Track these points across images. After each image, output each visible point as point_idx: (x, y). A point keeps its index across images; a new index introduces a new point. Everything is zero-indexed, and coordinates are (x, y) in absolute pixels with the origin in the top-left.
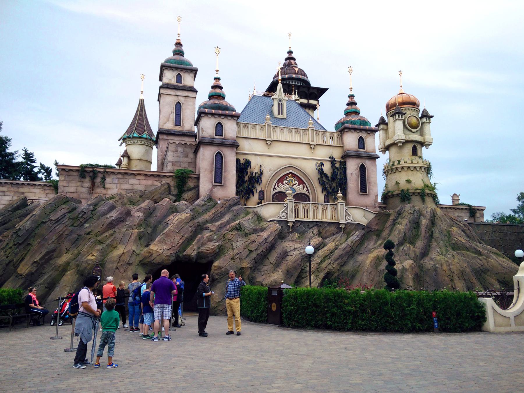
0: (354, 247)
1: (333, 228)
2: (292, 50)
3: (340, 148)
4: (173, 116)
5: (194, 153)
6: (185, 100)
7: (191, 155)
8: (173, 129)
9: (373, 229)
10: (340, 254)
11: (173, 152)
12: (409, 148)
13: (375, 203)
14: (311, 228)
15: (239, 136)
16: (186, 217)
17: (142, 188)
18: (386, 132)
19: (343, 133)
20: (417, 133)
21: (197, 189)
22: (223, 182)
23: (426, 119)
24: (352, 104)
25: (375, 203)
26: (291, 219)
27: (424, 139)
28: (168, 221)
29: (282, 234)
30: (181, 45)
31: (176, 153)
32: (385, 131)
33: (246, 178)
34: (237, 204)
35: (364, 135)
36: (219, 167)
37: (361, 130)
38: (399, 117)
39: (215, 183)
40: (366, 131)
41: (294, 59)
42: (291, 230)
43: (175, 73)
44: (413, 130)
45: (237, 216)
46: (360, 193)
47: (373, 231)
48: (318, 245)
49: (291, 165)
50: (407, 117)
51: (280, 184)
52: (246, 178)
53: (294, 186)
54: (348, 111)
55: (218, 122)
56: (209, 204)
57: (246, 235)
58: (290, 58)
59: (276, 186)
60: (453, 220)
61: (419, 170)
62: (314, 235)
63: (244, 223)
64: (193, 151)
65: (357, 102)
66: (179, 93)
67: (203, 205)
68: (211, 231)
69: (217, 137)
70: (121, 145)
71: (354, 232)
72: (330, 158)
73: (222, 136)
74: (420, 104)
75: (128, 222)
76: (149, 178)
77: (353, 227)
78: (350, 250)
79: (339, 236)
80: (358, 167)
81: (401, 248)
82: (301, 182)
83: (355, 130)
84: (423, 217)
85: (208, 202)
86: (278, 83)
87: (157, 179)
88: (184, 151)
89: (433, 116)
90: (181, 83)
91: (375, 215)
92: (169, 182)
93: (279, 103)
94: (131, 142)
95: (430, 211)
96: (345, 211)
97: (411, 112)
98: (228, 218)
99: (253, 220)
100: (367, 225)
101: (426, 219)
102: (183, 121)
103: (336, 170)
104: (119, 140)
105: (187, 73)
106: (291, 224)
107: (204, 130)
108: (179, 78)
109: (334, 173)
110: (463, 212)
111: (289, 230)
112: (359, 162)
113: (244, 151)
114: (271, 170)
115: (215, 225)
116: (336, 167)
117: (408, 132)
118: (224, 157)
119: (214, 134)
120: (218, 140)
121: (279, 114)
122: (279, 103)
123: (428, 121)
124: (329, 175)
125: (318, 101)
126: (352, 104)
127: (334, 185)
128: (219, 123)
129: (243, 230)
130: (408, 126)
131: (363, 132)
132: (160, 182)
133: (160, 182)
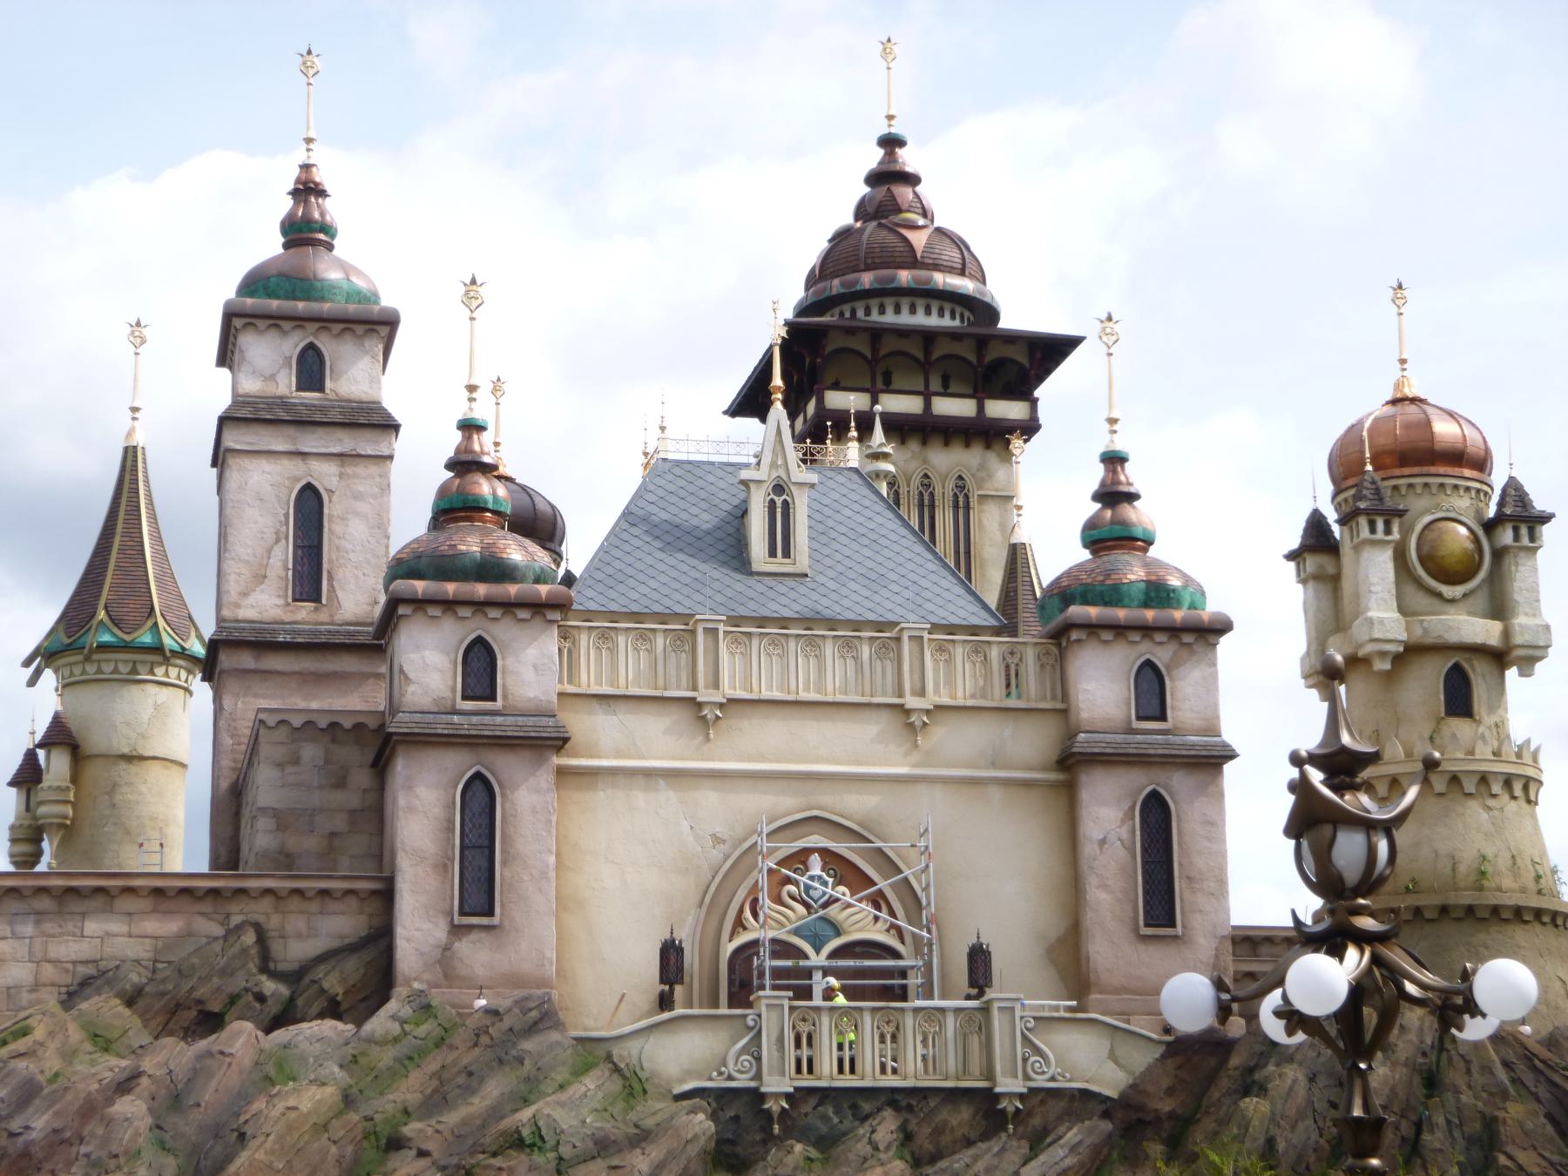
1: (961, 1118)
4: (283, 556)
5: (375, 764)
6: (341, 475)
7: (362, 778)
8: (288, 617)
12: (1426, 683)
15: (571, 689)
16: (319, 1101)
20: (1471, 600)
21: (382, 944)
22: (498, 910)
23: (1516, 530)
24: (1113, 496)
26: (778, 1084)
27: (1506, 634)
28: (246, 1122)
30: (322, 193)
34: (541, 1026)
35: (1161, 654)
37: (1147, 630)
38: (1373, 530)
39: (462, 913)
40: (1174, 631)
41: (912, 180)
43: (293, 344)
44: (1447, 591)
45: (537, 1079)
49: (815, 813)
54: (1104, 533)
55: (472, 636)
56: (422, 1030)
59: (748, 914)
61: (1473, 791)
63: (558, 1114)
64: (370, 755)
65: (1137, 486)
66: (312, 441)
67: (396, 1040)
68: (422, 1154)
69: (469, 705)
70: (32, 682)
71: (1062, 1129)
75: (88, 1143)
77: (1054, 1108)
79: (989, 1149)
80: (1132, 808)
83: (1120, 630)
85: (417, 1025)
86: (771, 403)
87: (207, 907)
88: (327, 761)
90: (321, 389)
92: (261, 919)
93: (772, 502)
94: (84, 672)
96: (1023, 1035)
98: (496, 1093)
99: (600, 1095)
100: (1123, 1095)
101: (1394, 1064)
102: (331, 578)
104: (27, 663)
105: (348, 337)
108: (311, 370)
112: (1139, 782)
113: (591, 756)
114: (724, 842)
115: (439, 1127)
117: (1419, 600)
120: (475, 719)
121: (773, 553)
122: (772, 502)
123: (1525, 541)
125: (1034, 402)
126: (1113, 496)
128: (480, 642)
129: (548, 1146)
131: (1160, 637)
132: (221, 917)
133: (221, 917)
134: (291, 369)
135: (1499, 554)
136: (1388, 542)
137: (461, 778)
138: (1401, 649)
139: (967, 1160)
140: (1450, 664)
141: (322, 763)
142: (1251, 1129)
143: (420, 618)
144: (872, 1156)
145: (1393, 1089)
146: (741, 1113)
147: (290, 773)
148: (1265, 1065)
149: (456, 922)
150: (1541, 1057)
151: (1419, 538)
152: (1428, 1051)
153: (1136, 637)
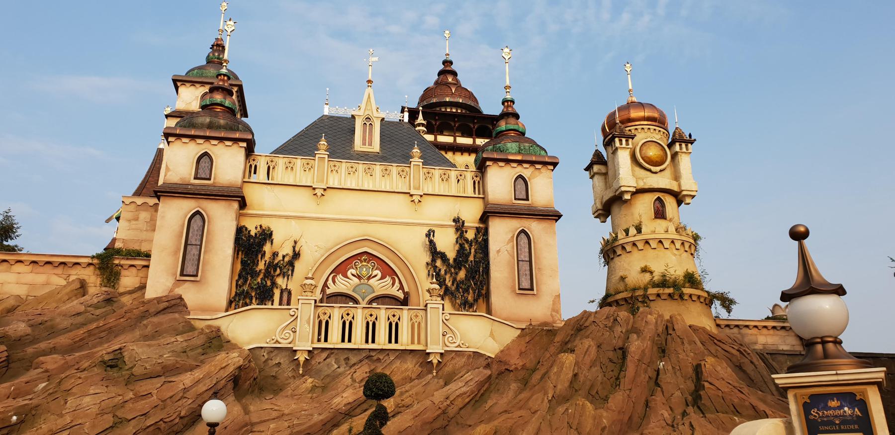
0: (452, 411)
2: (450, 58)
3: (481, 199)
9: (513, 367)
10: (404, 427)
11: (129, 221)
13: (554, 313)
14: (354, 365)
17: (22, 291)
18: (606, 179)
19: (483, 170)
20: (663, 173)
22: (200, 274)
23: (680, 145)
25: (554, 313)
29: (278, 381)
31: (134, 222)
32: (603, 177)
33: (261, 266)
35: (526, 171)
36: (194, 243)
38: (621, 144)
42: (301, 372)
44: (654, 169)
46: (518, 292)
47: (512, 371)
48: (349, 406)
50: (640, 144)
51: (340, 277)
52: (261, 266)
53: (372, 281)
57: (131, 380)
58: (447, 70)
59: (330, 281)
60: (715, 341)
62: (354, 381)
72: (454, 220)
73: (209, 179)
74: (665, 112)
76: (41, 269)
77: (461, 361)
78: (439, 416)
80: (513, 237)
81: (561, 409)
82: (388, 271)
84: (635, 336)
87: (59, 271)
89: (690, 133)
91: (519, 332)
92: (85, 277)
95: (654, 321)
97: (649, 134)
103: (466, 246)
106: (302, 357)
107: (171, 167)
109: (462, 253)
110: (777, 335)
111: (295, 370)
113: (259, 210)
116: (467, 240)
118: (209, 222)
119: (191, 175)
124: (451, 255)
127: (462, 274)
130: (641, 161)
131: (525, 165)
133: (65, 276)
134: (197, 100)
135: (674, 156)
136: (628, 148)
137: (189, 213)
138: (635, 190)
139: (407, 388)
140: (656, 197)
141: (149, 220)
142: (564, 369)
143: (178, 142)
144: (352, 385)
145: (643, 351)
146: (282, 361)
147: (133, 224)
148: (575, 340)
149: (177, 279)
150: (718, 339)
151: (642, 158)
152: (660, 334)
153: (515, 165)
